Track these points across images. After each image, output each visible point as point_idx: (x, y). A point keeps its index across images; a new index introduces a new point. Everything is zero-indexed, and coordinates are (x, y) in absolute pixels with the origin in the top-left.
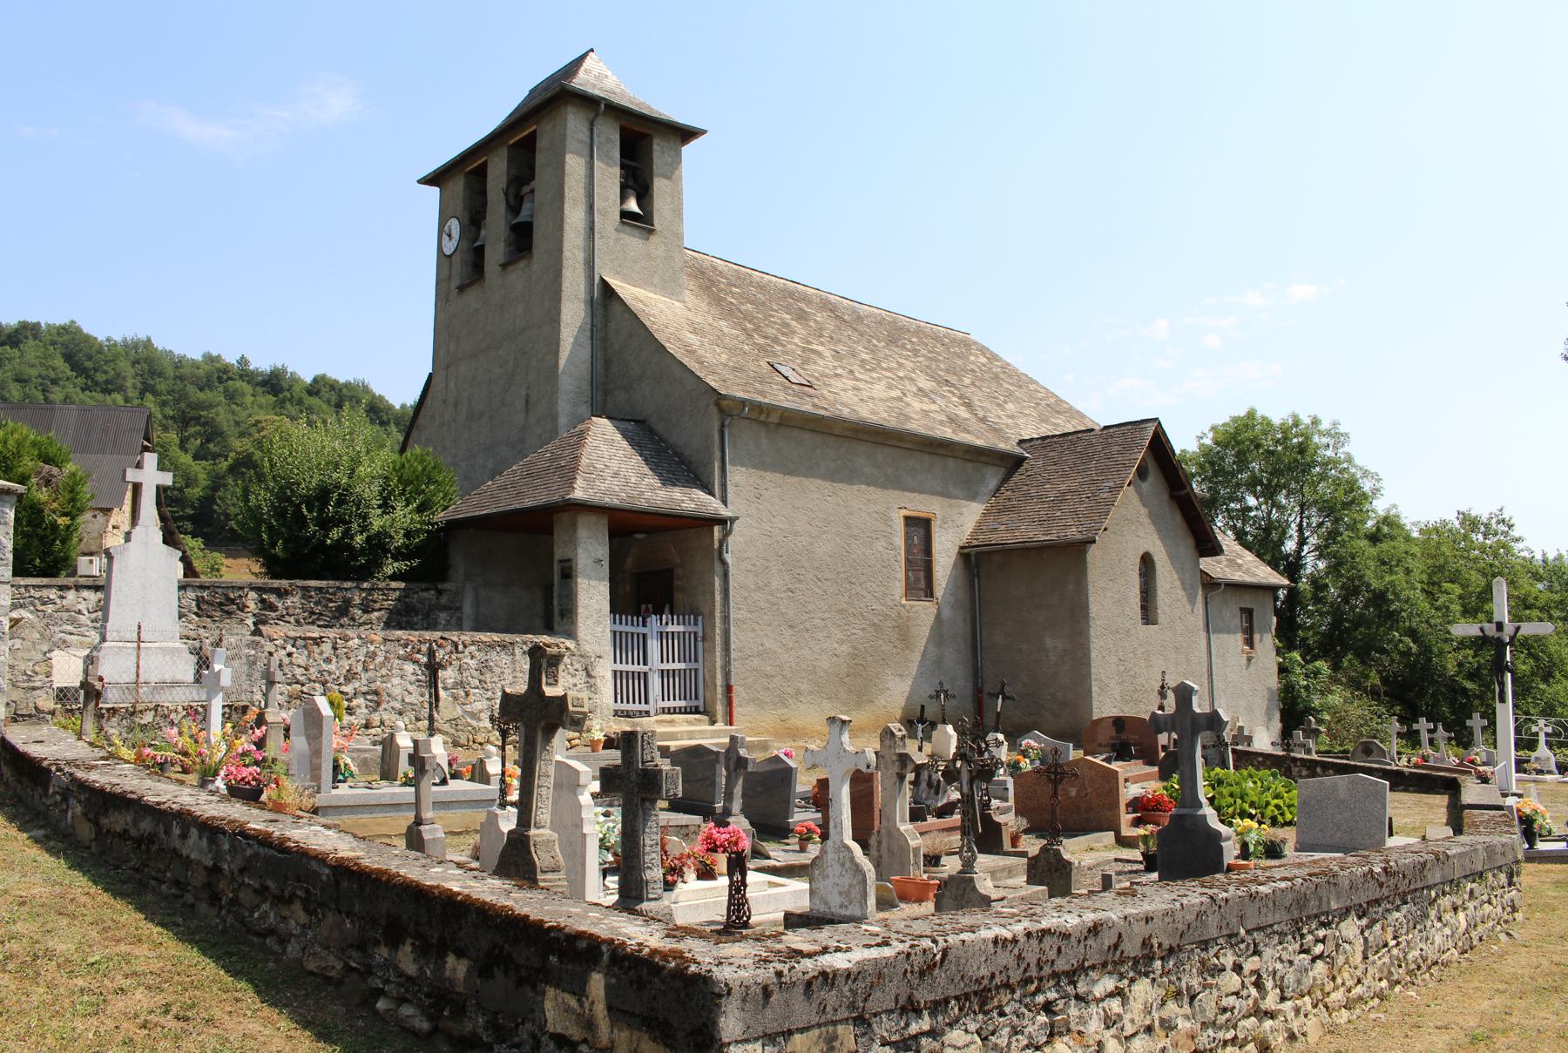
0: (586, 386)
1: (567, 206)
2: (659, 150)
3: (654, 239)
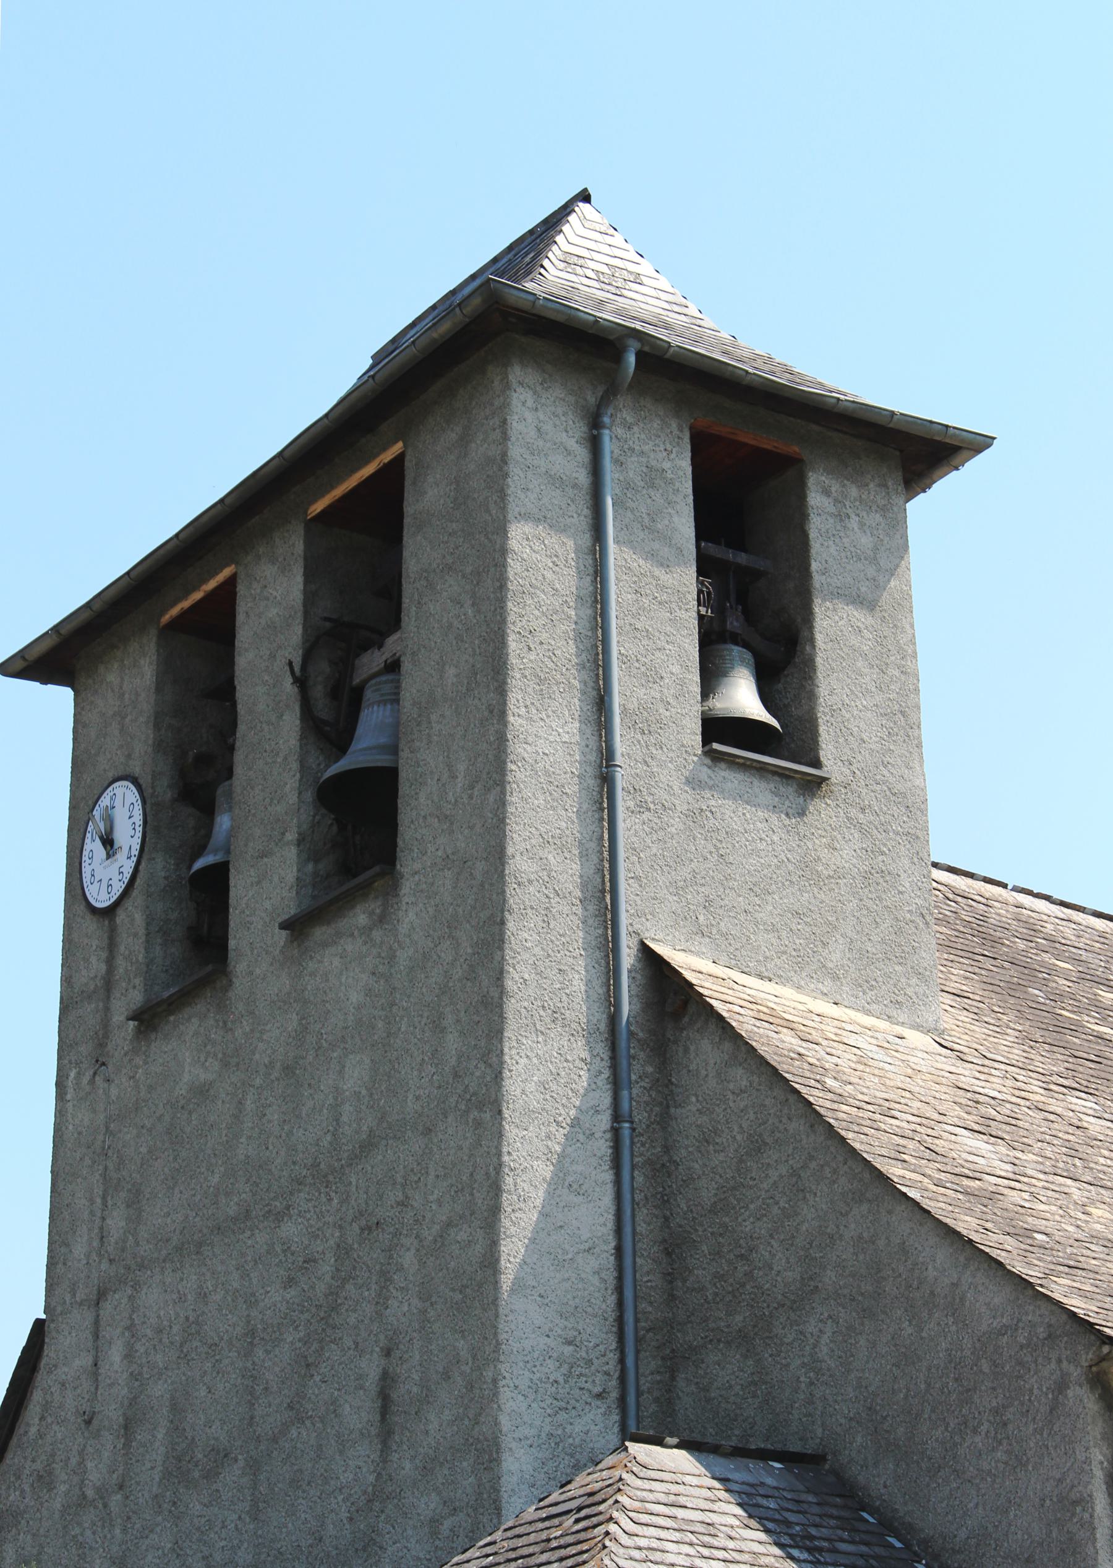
0: (598, 1334)
1: (516, 699)
2: (831, 512)
3: (823, 811)
